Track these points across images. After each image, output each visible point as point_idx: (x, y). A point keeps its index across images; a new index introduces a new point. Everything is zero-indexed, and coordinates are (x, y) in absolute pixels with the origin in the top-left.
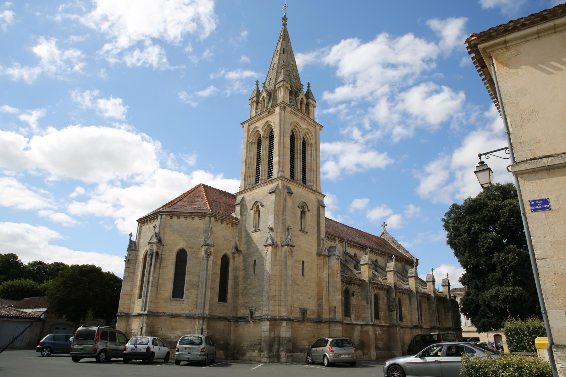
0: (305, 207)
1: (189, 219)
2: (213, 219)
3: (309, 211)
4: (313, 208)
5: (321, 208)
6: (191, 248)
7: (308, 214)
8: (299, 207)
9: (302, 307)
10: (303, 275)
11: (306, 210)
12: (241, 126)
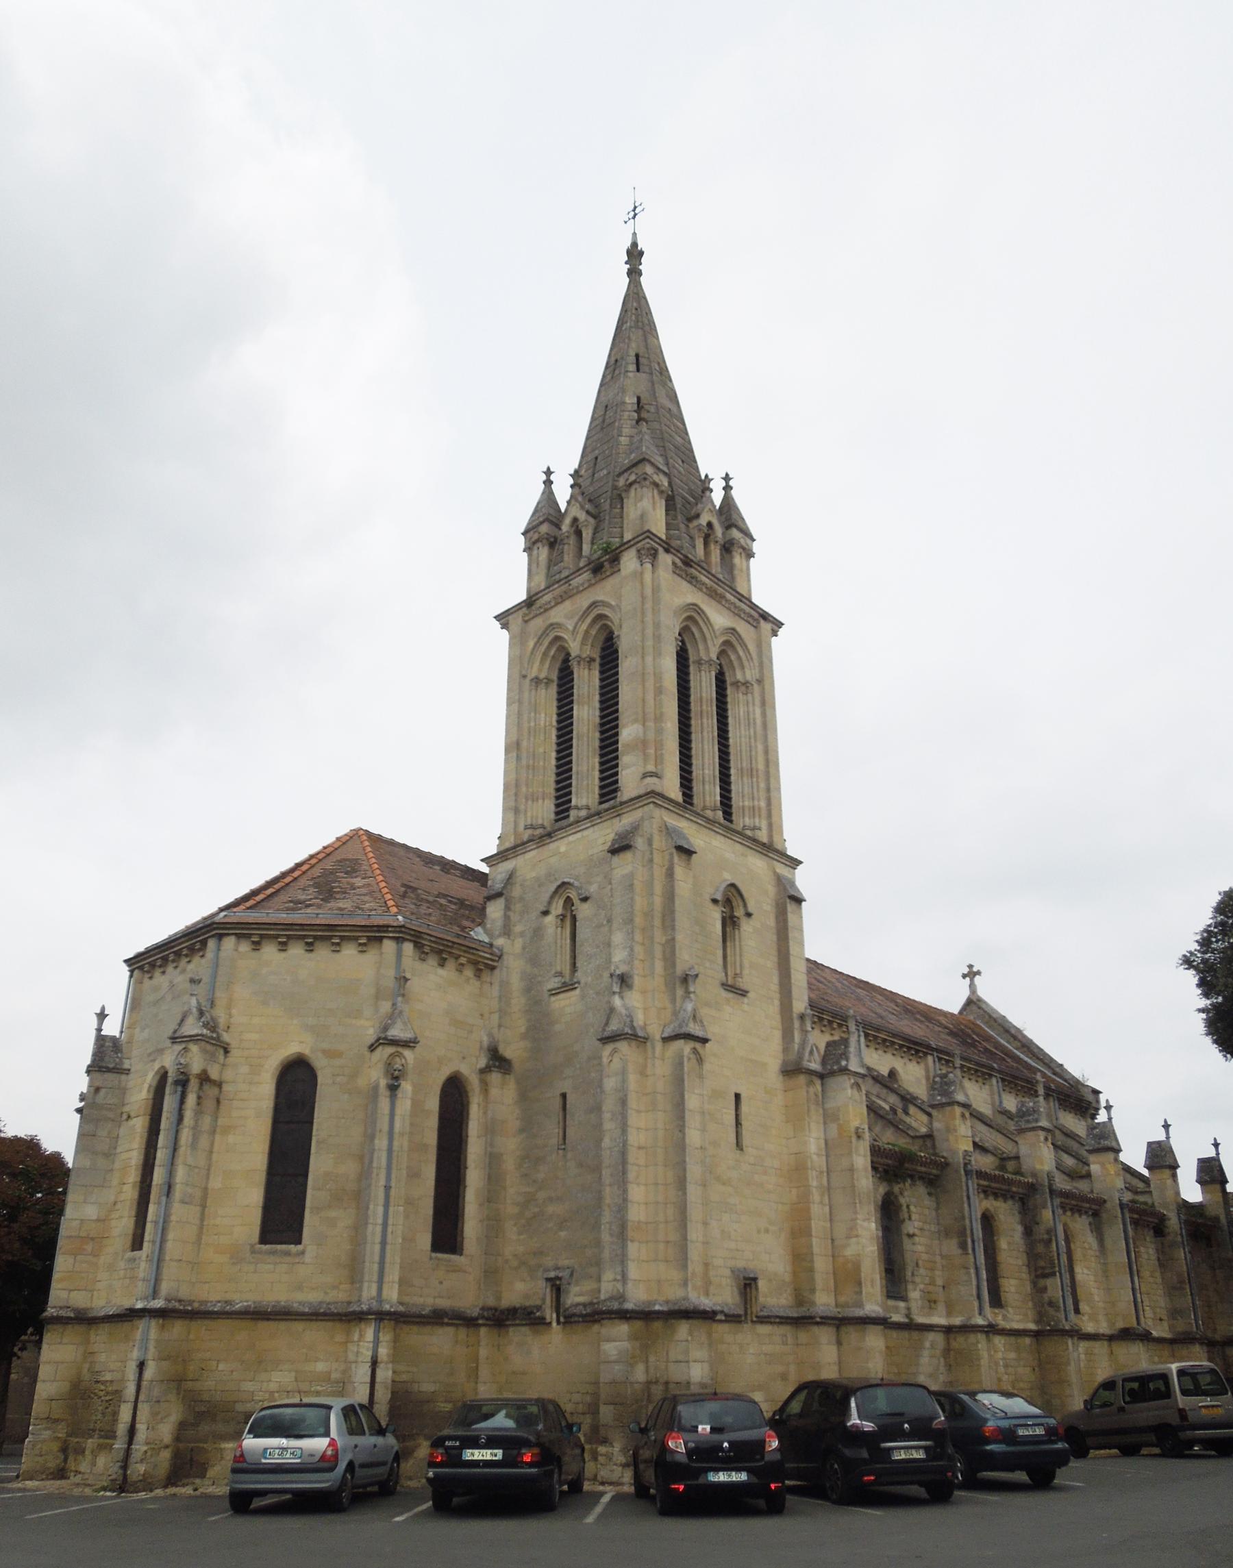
0: (736, 902)
1: (323, 952)
2: (408, 947)
3: (749, 915)
4: (761, 900)
5: (791, 907)
6: (330, 1054)
7: (746, 927)
8: (715, 901)
9: (740, 1264)
10: (739, 1145)
11: (739, 912)
12: (497, 624)
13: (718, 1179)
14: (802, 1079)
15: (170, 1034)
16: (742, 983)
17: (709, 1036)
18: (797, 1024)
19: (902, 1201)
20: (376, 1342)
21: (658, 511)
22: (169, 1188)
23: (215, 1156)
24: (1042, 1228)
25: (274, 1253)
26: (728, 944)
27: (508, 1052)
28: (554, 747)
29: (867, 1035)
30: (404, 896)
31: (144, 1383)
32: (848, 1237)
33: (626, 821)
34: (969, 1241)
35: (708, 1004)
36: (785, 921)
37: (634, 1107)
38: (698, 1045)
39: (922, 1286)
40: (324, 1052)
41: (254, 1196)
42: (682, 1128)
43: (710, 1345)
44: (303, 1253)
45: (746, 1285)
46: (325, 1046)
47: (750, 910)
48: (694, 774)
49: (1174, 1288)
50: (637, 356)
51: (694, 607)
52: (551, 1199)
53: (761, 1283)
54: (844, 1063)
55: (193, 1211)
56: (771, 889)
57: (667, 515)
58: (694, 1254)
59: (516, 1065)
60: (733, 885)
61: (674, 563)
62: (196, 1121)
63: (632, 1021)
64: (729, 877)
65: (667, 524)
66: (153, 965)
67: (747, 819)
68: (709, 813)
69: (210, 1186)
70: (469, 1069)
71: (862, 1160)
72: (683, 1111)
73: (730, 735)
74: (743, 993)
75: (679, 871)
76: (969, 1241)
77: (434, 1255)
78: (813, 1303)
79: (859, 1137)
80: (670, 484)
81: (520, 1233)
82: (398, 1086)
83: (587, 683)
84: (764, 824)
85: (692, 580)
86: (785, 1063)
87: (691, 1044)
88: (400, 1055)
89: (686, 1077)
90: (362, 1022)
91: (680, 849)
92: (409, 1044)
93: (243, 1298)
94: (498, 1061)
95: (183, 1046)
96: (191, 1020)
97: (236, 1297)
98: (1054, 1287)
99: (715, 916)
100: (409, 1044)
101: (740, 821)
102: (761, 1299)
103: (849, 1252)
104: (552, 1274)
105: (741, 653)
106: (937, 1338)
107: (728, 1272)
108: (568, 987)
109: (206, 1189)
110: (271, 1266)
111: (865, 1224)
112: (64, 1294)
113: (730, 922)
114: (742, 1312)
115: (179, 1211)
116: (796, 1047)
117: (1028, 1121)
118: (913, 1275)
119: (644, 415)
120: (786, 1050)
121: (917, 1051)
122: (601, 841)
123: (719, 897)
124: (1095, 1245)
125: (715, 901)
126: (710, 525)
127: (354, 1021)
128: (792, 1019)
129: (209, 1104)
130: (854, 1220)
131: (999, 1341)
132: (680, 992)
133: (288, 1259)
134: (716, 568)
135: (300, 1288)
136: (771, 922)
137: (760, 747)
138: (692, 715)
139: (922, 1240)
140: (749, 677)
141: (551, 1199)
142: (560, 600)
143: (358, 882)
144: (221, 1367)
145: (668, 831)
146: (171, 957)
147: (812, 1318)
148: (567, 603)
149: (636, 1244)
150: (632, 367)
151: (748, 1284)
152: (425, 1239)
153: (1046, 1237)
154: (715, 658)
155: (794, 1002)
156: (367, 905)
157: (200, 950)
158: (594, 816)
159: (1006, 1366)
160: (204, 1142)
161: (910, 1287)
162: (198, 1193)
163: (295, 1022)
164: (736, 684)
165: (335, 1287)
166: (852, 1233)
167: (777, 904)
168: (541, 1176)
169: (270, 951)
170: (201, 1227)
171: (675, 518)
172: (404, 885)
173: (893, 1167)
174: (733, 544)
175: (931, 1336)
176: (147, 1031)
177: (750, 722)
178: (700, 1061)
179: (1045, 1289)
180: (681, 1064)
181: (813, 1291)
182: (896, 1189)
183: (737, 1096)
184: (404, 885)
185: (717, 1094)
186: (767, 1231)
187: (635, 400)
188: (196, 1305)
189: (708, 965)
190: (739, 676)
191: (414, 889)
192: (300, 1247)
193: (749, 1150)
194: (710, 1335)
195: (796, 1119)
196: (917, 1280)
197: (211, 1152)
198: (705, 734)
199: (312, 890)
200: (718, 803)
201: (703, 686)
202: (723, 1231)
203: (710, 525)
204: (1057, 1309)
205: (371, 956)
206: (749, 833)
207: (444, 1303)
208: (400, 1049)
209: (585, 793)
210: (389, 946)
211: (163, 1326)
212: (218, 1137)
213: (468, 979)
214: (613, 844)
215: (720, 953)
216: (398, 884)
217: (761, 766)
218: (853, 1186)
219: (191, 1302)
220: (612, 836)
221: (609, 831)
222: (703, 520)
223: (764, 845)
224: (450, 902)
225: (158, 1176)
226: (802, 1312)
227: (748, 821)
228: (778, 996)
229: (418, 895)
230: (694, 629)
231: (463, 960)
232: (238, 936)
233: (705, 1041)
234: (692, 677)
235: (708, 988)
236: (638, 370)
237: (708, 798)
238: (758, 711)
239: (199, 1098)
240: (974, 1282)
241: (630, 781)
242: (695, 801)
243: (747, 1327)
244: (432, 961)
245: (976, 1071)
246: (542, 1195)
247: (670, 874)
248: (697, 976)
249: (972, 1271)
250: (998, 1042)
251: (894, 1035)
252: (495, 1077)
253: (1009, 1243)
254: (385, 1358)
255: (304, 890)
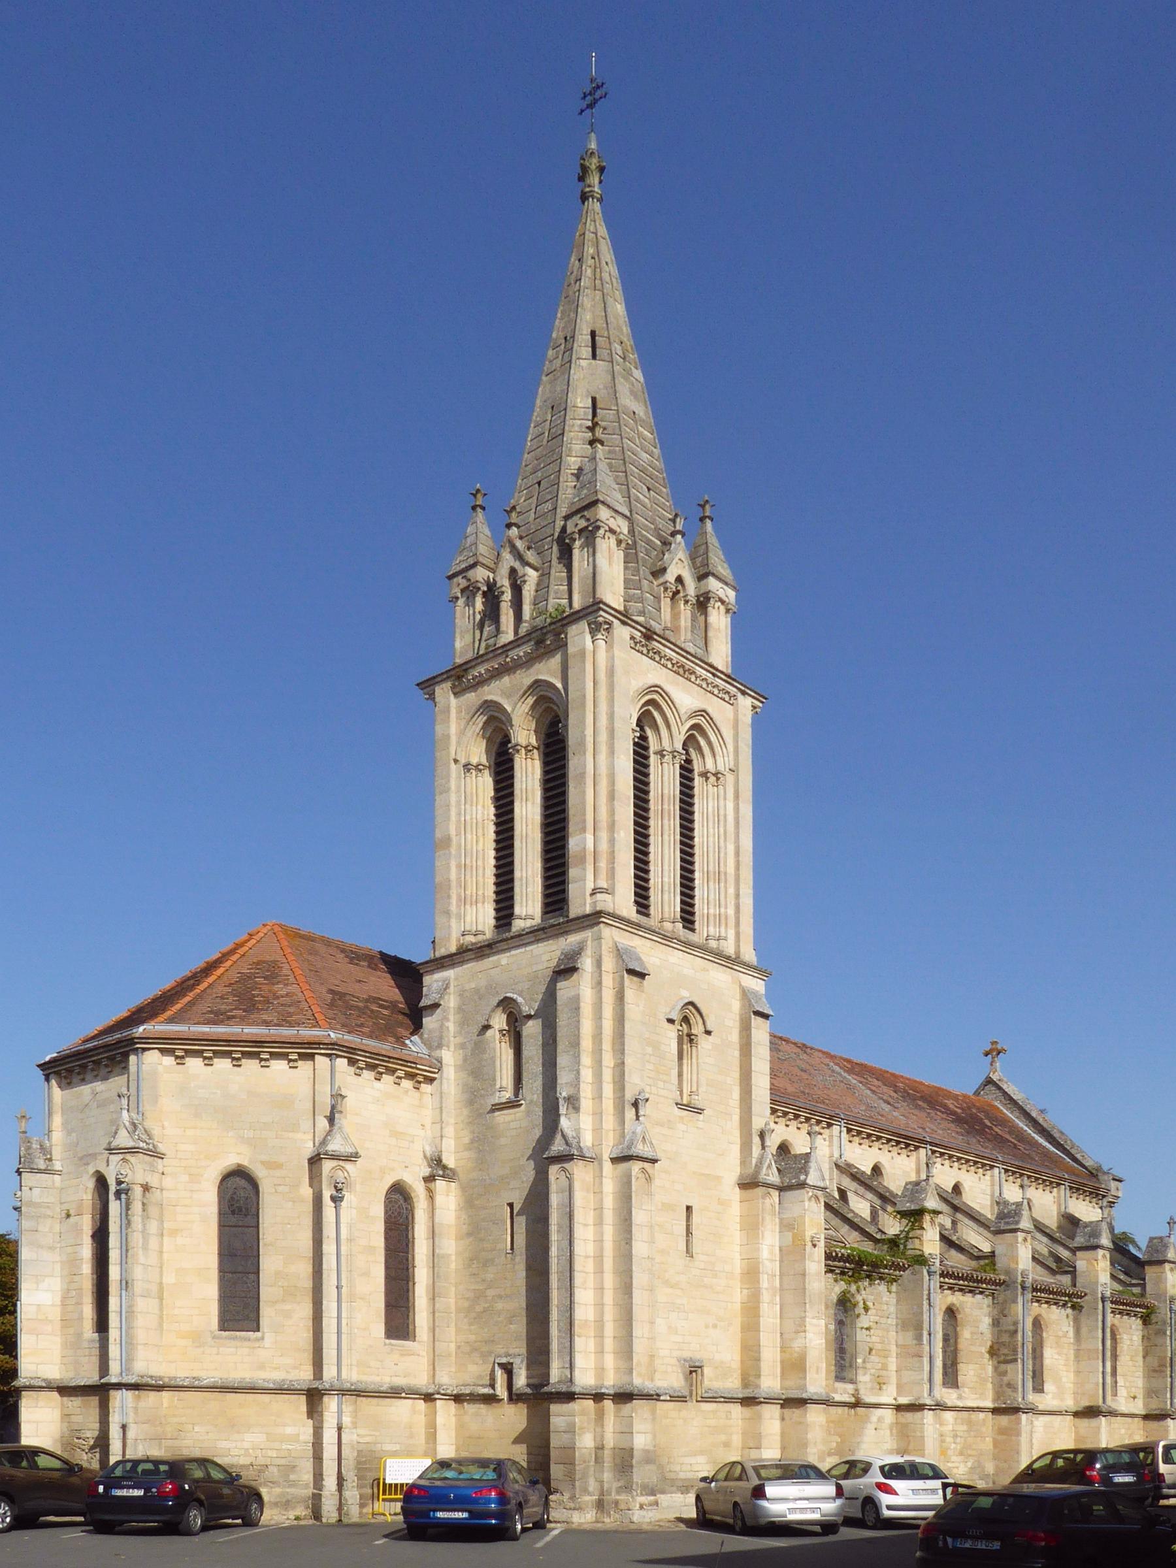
0: (695, 1020)
1: (251, 1065)
2: (342, 1063)
3: (708, 1033)
7: (704, 1043)
8: (671, 1021)
9: (687, 1354)
10: (689, 1251)
11: (697, 1029)
13: (667, 1283)
14: (760, 1191)
15: (105, 1146)
16: (698, 1101)
17: (659, 1155)
18: (756, 1140)
19: (859, 1298)
20: (340, 1413)
21: (615, 566)
22: (126, 1284)
23: (165, 1256)
24: (1009, 1319)
25: (235, 1338)
26: (685, 1061)
27: (450, 1160)
28: (493, 845)
29: (849, 1131)
30: (332, 1005)
31: (129, 1442)
32: (797, 1332)
33: (573, 939)
34: (925, 1333)
35: (660, 1124)
36: (749, 1036)
37: (581, 1221)
38: (647, 1165)
39: (873, 1371)
40: (263, 1163)
41: (209, 1291)
42: (629, 1241)
43: (654, 1419)
44: (263, 1338)
45: (691, 1372)
46: (264, 1158)
47: (709, 1028)
48: (651, 882)
49: (1155, 1371)
50: (593, 334)
51: (655, 688)
52: (500, 1297)
53: (706, 1370)
54: (802, 1177)
55: (153, 1303)
56: (736, 1005)
57: (626, 568)
58: (639, 1346)
59: (461, 1174)
60: (691, 1003)
61: (632, 638)
62: (144, 1225)
63: (579, 1142)
64: (687, 996)
65: (626, 581)
66: (70, 1071)
67: (711, 929)
68: (668, 926)
69: (164, 1281)
70: (414, 1179)
71: (815, 1262)
72: (630, 1225)
73: (696, 833)
74: (699, 1111)
75: (629, 994)
76: (925, 1333)
77: (387, 1341)
78: (758, 1386)
79: (815, 1246)
80: (632, 531)
81: (471, 1324)
82: (343, 1198)
83: (529, 774)
84: (731, 934)
85: (654, 655)
86: (741, 1176)
87: (640, 1164)
88: (342, 1169)
89: (633, 1195)
90: (299, 1136)
91: (631, 972)
92: (352, 1157)
93: (211, 1375)
94: (438, 1169)
95: (121, 1156)
96: (123, 1133)
97: (203, 1374)
98: (1018, 1372)
99: (670, 1036)
100: (352, 1157)
101: (704, 929)
102: (706, 1383)
103: (797, 1345)
104: (504, 1360)
105: (713, 738)
106: (888, 1415)
107: (674, 1361)
108: (512, 1104)
109: (161, 1283)
110: (233, 1350)
111: (815, 1321)
112: (32, 1367)
113: (688, 1039)
114: (686, 1393)
115: (141, 1304)
116: (754, 1161)
117: (1008, 1223)
118: (864, 1362)
119: (599, 433)
120: (743, 1163)
121: (907, 1145)
122: (546, 957)
123: (675, 1016)
124: (1071, 1334)
125: (671, 1021)
126: (679, 579)
127: (291, 1135)
128: (751, 1135)
129: (153, 1211)
130: (803, 1319)
131: (948, 1416)
132: (630, 1113)
133: (247, 1343)
134: (685, 637)
135: (262, 1367)
136: (735, 1037)
137: (731, 848)
138: (652, 814)
139: (880, 1333)
140: (721, 768)
141: (500, 1297)
142: (496, 674)
143: (280, 989)
144: (197, 1429)
145: (620, 953)
146: (90, 1066)
147: (755, 1398)
148: (506, 680)
149: (583, 1338)
150: (586, 352)
151: (694, 1370)
152: (379, 1328)
153: (1012, 1328)
154: (679, 746)
155: (753, 1118)
156: (294, 1018)
157: (120, 1062)
158: (538, 934)
159: (955, 1436)
160: (153, 1243)
161: (860, 1371)
162: (154, 1288)
163: (230, 1134)
164: (705, 775)
165: (295, 1368)
166: (801, 1328)
167: (741, 1020)
168: (490, 1276)
169: (194, 1064)
170: (161, 1317)
171: (637, 571)
172: (331, 991)
173: (850, 1267)
174: (708, 599)
175: (879, 1412)
176: (74, 1135)
177: (720, 818)
178: (649, 1179)
179: (1005, 1373)
180: (629, 1183)
181: (759, 1376)
182: (853, 1288)
183: (689, 1209)
184: (331, 991)
185: (668, 1207)
186: (715, 1326)
187: (589, 403)
188: (166, 1380)
189: (661, 1084)
190: (710, 765)
191: (342, 995)
192: (258, 1334)
193: (700, 1258)
194: (653, 1412)
195: (752, 1227)
196: (868, 1365)
197: (161, 1252)
198: (666, 837)
199: (231, 999)
200: (678, 915)
201: (664, 780)
202: (670, 1327)
203: (679, 579)
204: (1015, 1389)
205: (305, 1067)
206: (713, 944)
207: (400, 1381)
208: (341, 1163)
209: (529, 903)
210: (322, 1062)
211: (139, 1397)
212: (166, 1239)
213: (407, 1092)
214: (558, 965)
215: (675, 1072)
216: (324, 990)
217: (731, 869)
218: (805, 1289)
219: (161, 1378)
220: (558, 953)
221: (554, 947)
222: (670, 576)
223: (728, 958)
224: (381, 1006)
225: (114, 1272)
226: (748, 1393)
227: (712, 931)
228: (738, 1110)
229: (346, 1002)
230: (656, 714)
231: (401, 1074)
232: (163, 1051)
233: (654, 1161)
234: (652, 770)
235: (661, 1107)
236: (594, 356)
237: (666, 909)
238: (730, 805)
239: (144, 1204)
240: (927, 1368)
241: (580, 902)
242: (652, 910)
243: (692, 1405)
244: (368, 1075)
245: (976, 1163)
246: (490, 1293)
247: (620, 997)
248: (647, 1100)
249: (926, 1360)
250: (1017, 1127)
251: (881, 1130)
252: (440, 1184)
253: (972, 1333)
254: (349, 1425)
255: (222, 998)
